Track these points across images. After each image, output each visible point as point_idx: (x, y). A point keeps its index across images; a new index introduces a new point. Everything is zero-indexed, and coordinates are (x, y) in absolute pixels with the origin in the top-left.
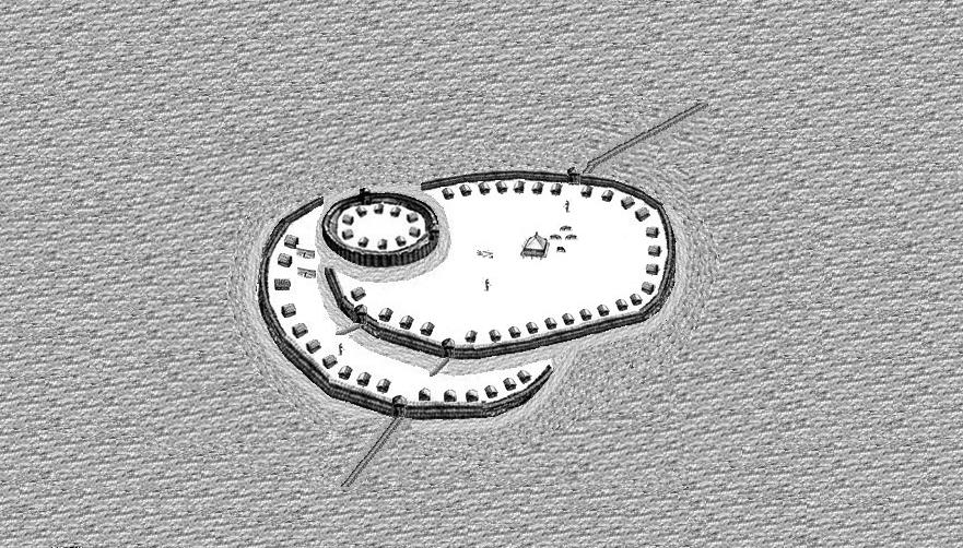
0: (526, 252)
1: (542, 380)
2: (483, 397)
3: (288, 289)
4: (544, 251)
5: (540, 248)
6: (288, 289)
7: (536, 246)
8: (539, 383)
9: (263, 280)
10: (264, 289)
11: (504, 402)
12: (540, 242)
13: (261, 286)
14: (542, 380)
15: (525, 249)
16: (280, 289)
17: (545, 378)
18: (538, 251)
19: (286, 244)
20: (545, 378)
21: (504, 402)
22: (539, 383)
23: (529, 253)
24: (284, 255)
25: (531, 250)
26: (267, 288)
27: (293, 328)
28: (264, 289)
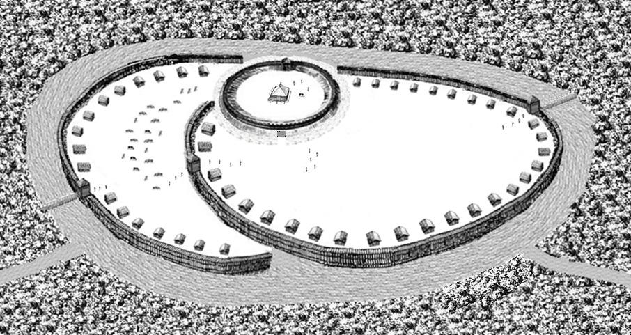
0: (272, 98)
1: (559, 152)
2: (78, 141)
3: (84, 152)
4: (287, 97)
5: (284, 95)
6: (84, 152)
7: (280, 93)
8: (557, 156)
9: (63, 155)
10: (66, 162)
11: (536, 186)
12: (284, 91)
13: (63, 161)
14: (559, 152)
15: (271, 96)
16: (78, 153)
17: (560, 149)
18: (282, 97)
19: (203, 131)
20: (560, 149)
21: (536, 186)
22: (557, 156)
23: (274, 98)
24: (537, 162)
25: (276, 96)
26: (69, 160)
27: (105, 196)
28: (66, 162)
